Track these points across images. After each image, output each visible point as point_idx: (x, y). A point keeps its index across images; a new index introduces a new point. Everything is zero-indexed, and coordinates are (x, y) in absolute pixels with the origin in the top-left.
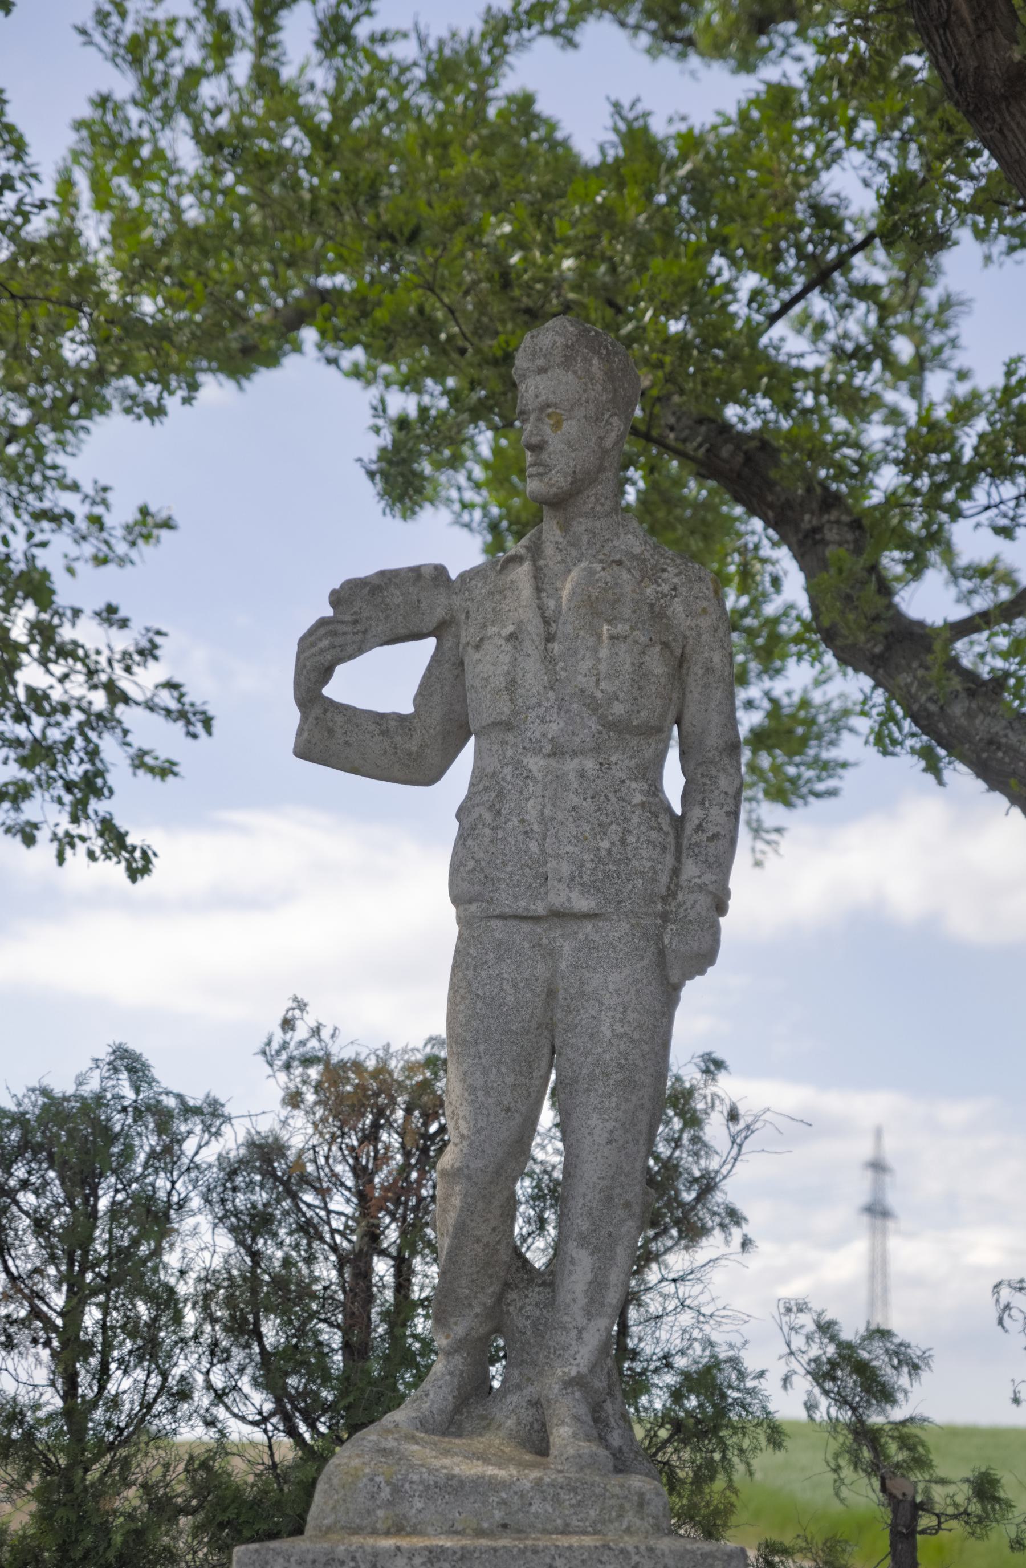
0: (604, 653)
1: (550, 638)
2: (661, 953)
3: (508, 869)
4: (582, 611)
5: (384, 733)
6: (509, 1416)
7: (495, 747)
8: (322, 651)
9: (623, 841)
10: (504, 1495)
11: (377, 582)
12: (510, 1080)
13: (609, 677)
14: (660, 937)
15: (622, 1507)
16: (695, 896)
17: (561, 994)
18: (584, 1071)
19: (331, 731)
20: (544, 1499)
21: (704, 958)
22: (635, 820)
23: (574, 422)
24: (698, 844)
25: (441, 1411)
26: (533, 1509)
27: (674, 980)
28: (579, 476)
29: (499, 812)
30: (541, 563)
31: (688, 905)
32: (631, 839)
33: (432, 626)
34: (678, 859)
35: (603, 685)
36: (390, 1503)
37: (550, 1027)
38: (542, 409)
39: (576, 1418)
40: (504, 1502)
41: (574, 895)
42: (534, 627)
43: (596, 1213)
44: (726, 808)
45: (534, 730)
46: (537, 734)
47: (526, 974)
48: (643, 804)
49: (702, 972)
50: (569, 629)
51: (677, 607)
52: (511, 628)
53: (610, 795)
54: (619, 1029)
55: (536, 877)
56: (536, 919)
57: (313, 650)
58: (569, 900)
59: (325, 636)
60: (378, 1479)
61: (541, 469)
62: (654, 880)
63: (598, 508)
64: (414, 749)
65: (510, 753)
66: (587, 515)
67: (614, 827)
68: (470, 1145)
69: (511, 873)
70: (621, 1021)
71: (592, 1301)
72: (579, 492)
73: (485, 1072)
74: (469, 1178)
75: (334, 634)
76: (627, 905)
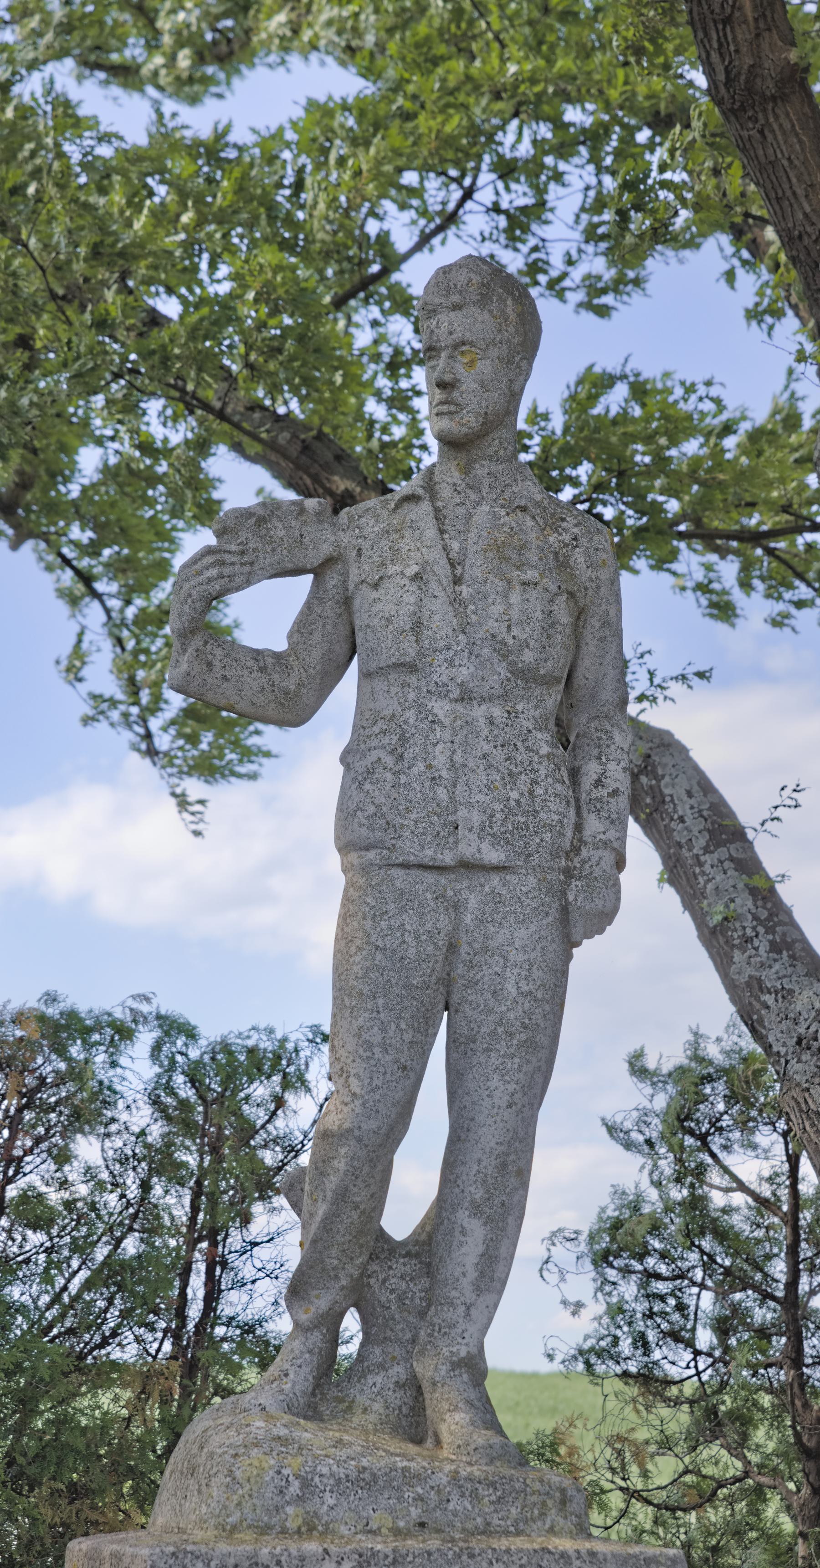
0: (515, 599)
1: (457, 581)
2: (565, 910)
3: (413, 816)
4: (490, 555)
5: (263, 669)
6: (376, 1395)
7: (394, 690)
8: (210, 580)
9: (531, 792)
10: (420, 1491)
11: (261, 512)
12: (408, 1037)
13: (520, 623)
14: (564, 895)
15: (544, 1504)
16: (600, 852)
17: (464, 949)
18: (484, 1030)
19: (209, 665)
20: (463, 1495)
21: (603, 918)
22: (543, 771)
23: (488, 362)
24: (599, 800)
25: (304, 1393)
26: (451, 1506)
27: (575, 937)
28: (490, 418)
29: (401, 757)
30: (439, 504)
31: (594, 861)
32: (539, 791)
33: (315, 560)
34: (578, 813)
35: (515, 631)
36: (300, 1499)
37: (447, 982)
38: (455, 347)
39: (468, 1402)
40: (420, 1498)
41: (485, 846)
42: (442, 568)
43: (491, 1181)
44: (623, 764)
45: (442, 673)
46: (445, 678)
47: (429, 926)
48: (548, 756)
49: (601, 931)
50: (477, 572)
51: (578, 558)
52: (414, 569)
53: (519, 744)
54: (525, 988)
55: (445, 825)
56: (441, 869)
57: (200, 579)
58: (479, 851)
59: (212, 565)
60: (285, 1472)
61: (453, 408)
62: (561, 835)
63: (502, 452)
64: (292, 687)
65: (412, 696)
66: (491, 458)
67: (523, 777)
68: (364, 1104)
69: (416, 821)
70: (526, 978)
71: (482, 1275)
72: (487, 434)
73: (384, 1028)
74: (359, 1140)
75: (222, 563)
76: (535, 859)
